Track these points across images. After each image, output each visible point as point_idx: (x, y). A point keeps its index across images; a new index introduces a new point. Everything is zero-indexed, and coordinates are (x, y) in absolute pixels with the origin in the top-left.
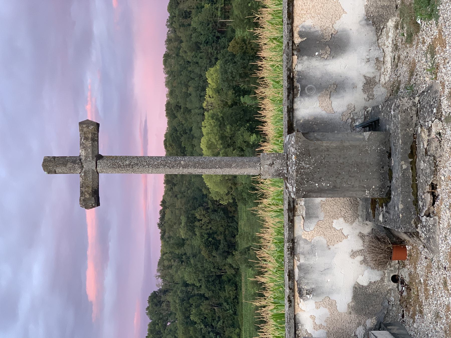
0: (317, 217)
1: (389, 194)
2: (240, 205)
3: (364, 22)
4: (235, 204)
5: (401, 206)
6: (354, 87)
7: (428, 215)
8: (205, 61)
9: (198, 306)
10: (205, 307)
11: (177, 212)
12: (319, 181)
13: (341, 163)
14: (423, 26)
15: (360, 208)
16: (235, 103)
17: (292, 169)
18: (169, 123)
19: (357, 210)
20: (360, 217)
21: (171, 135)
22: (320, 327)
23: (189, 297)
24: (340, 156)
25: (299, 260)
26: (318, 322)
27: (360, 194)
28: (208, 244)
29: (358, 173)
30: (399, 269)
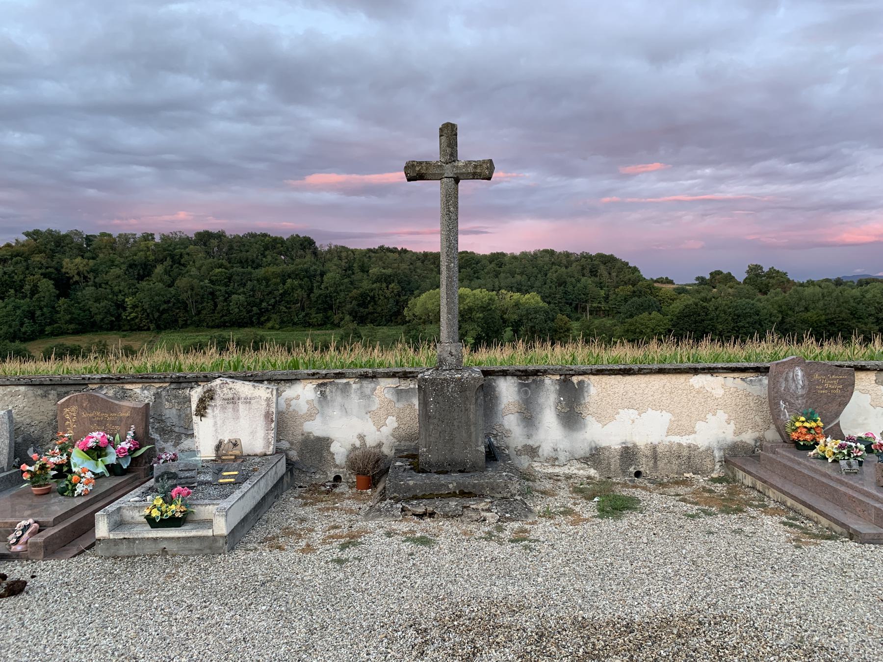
0: (398, 401)
1: (423, 471)
2: (403, 328)
3: (594, 445)
4: (404, 322)
5: (411, 483)
6: (529, 436)
7: (403, 510)
8: (546, 290)
9: (301, 286)
10: (299, 293)
11: (396, 265)
14: (591, 503)
15: (408, 443)
16: (505, 321)
17: (447, 375)
18: (485, 256)
19: (406, 440)
21: (473, 258)
22: (289, 405)
23: (309, 277)
25: (355, 383)
26: (293, 402)
27: (423, 442)
28: (364, 295)
30: (348, 482)
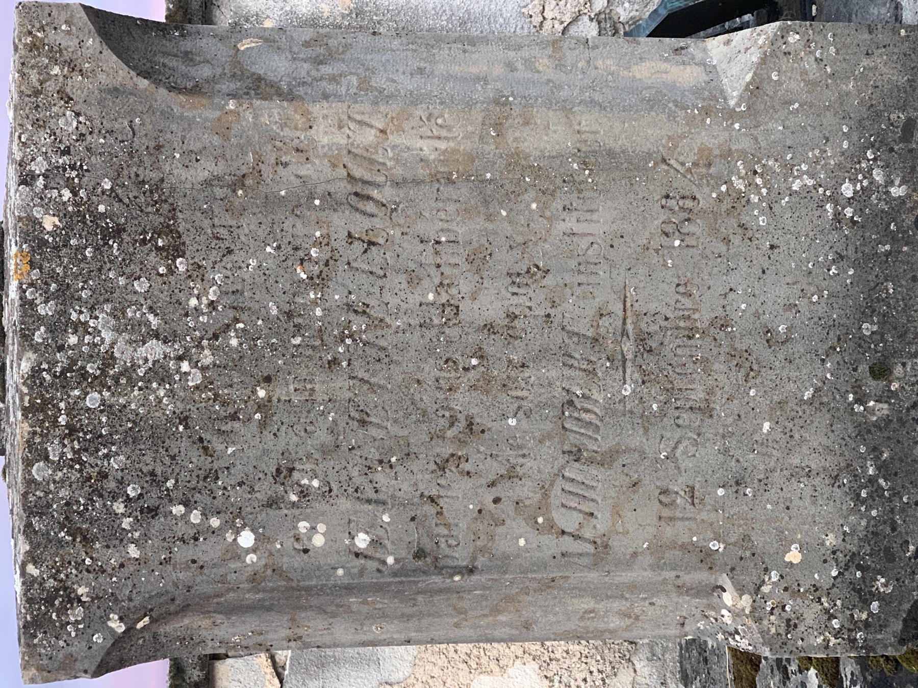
12: (272, 503)
13: (489, 328)
20: (644, 653)
24: (478, 260)
29: (646, 422)
